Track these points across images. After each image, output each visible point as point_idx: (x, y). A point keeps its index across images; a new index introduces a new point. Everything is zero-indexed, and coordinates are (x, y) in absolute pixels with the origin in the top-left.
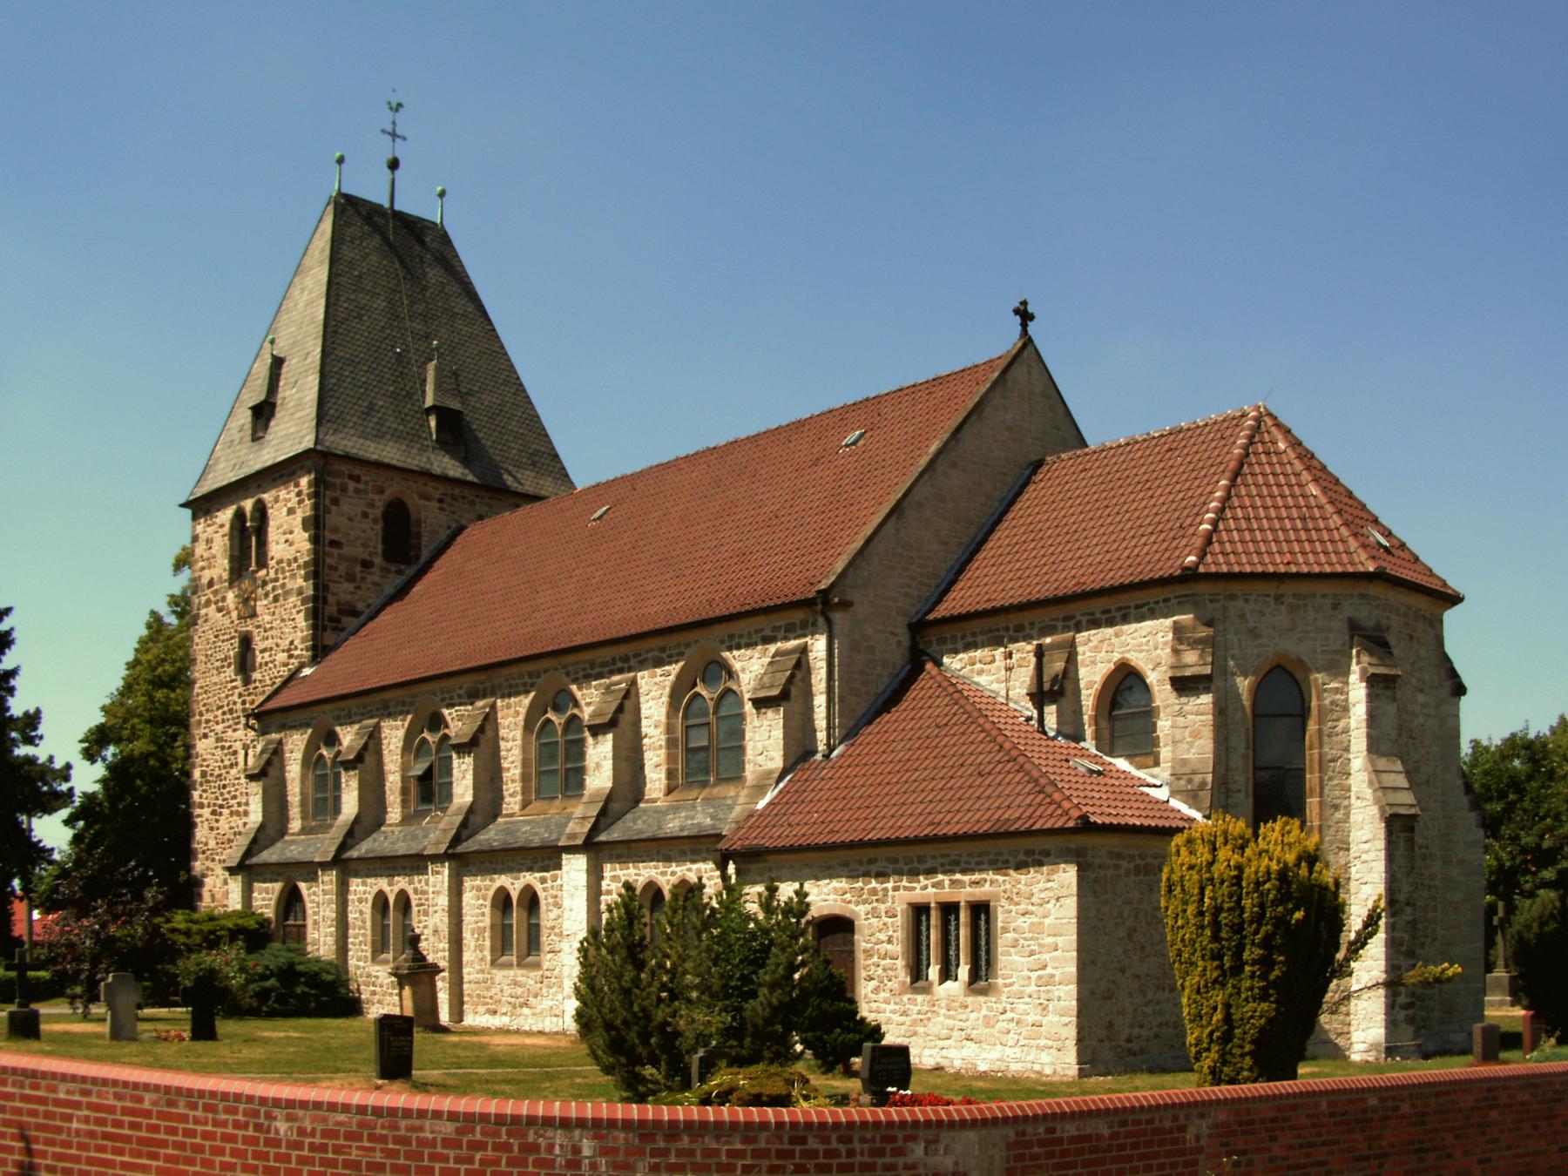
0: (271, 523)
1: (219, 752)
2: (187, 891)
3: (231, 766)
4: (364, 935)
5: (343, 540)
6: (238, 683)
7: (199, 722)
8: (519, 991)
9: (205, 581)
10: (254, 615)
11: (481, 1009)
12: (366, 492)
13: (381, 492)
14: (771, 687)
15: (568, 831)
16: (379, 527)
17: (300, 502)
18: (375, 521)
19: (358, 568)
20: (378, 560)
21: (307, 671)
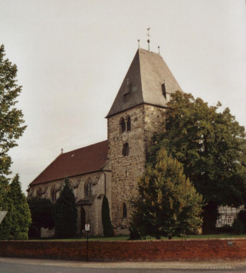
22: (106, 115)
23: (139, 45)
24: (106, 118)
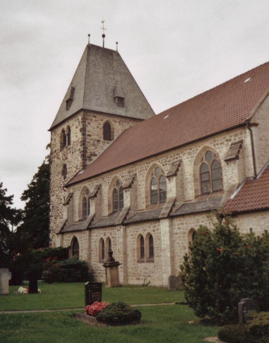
0: (71, 131)
1: (57, 199)
2: (46, 241)
3: (60, 203)
4: (97, 253)
5: (91, 134)
6: (63, 178)
7: (52, 191)
8: (147, 271)
9: (54, 151)
10: (67, 158)
11: (134, 278)
12: (98, 121)
13: (102, 120)
14: (231, 155)
15: (162, 212)
16: (102, 130)
17: (79, 124)
18: (101, 129)
19: (96, 142)
20: (102, 140)
21: (81, 172)
22: (49, 128)
23: (89, 41)
24: (49, 130)
